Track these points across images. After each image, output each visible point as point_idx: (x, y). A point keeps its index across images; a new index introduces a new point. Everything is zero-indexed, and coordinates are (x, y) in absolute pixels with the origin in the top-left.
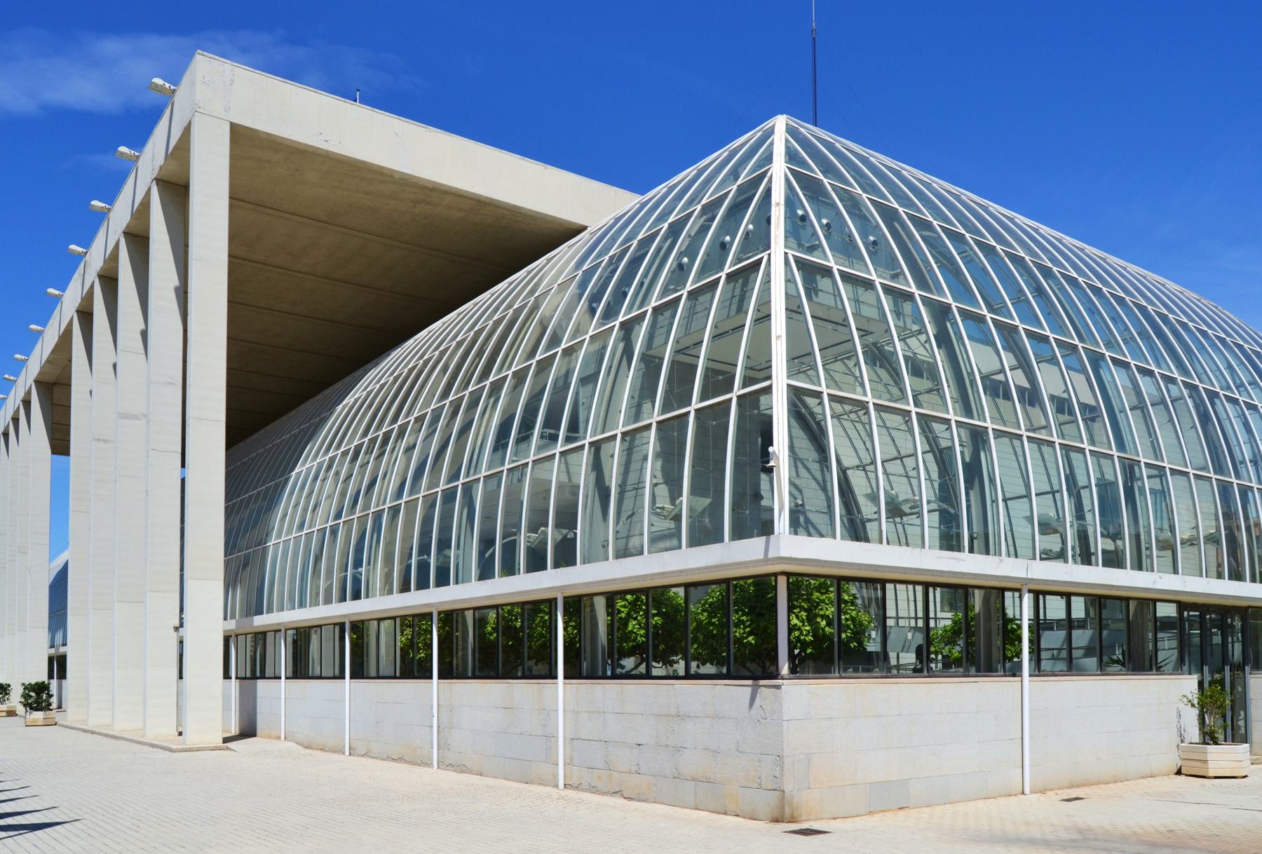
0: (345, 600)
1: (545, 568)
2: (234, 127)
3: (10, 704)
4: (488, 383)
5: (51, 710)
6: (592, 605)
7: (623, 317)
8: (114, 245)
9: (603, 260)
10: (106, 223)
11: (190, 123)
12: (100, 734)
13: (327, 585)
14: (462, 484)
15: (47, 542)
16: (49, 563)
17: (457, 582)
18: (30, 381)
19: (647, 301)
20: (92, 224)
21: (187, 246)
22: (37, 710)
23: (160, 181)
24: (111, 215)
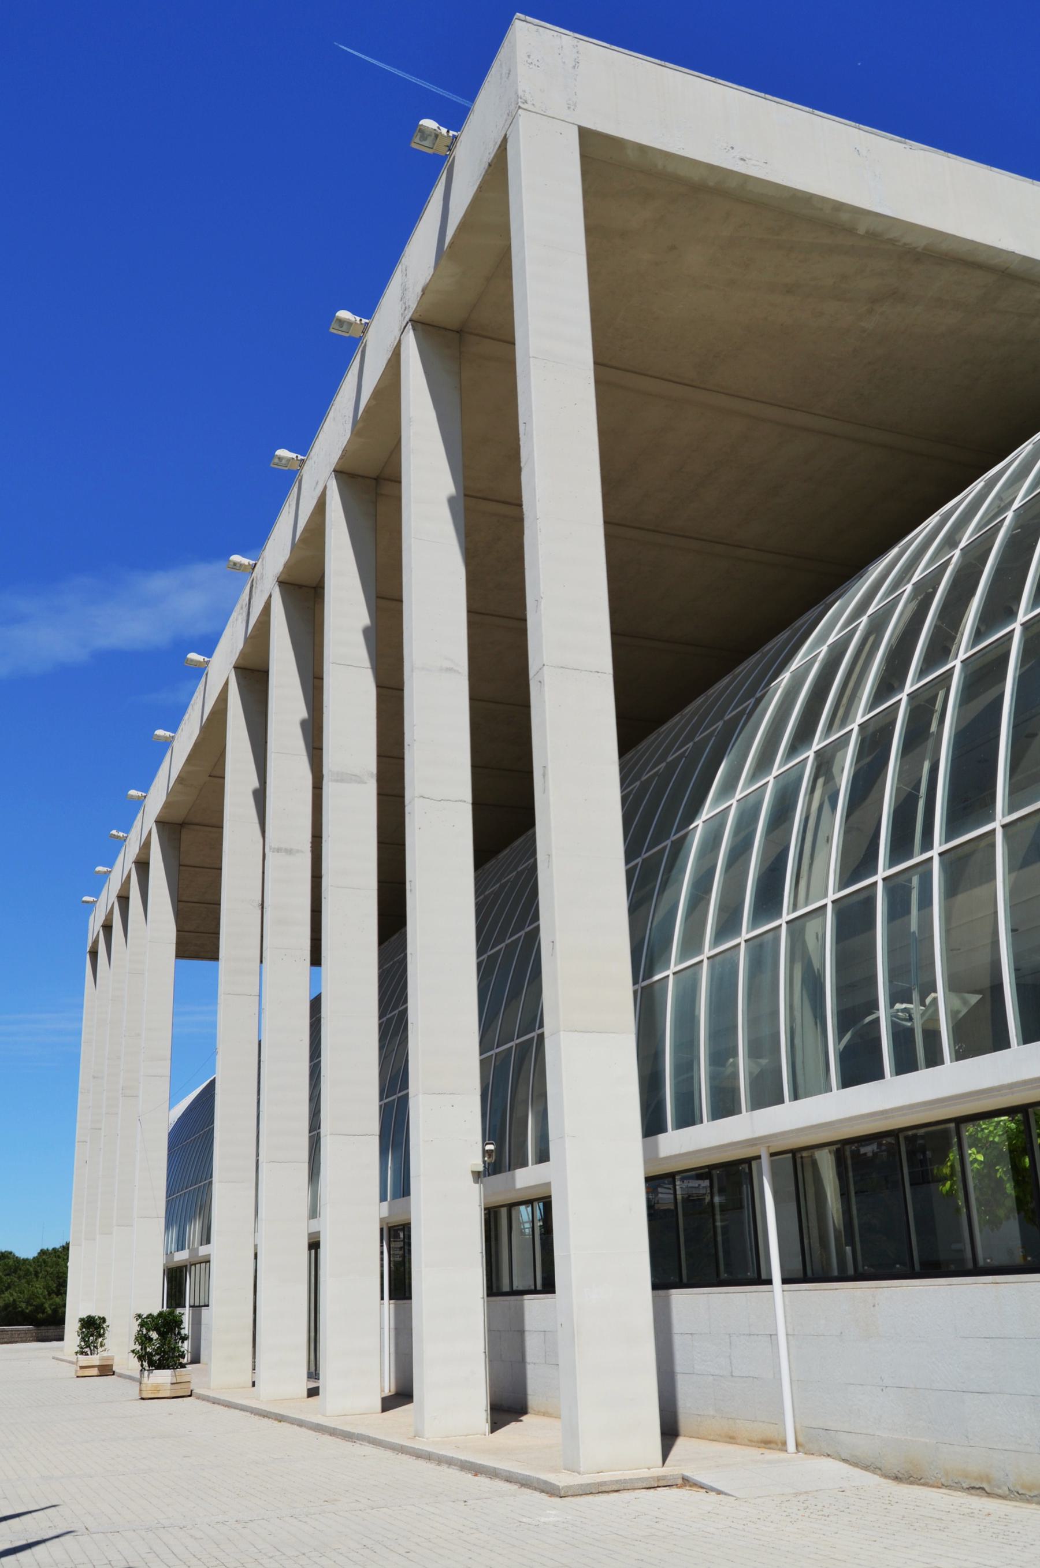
0: (940, 1061)
1: (1006, 1045)
2: (586, 135)
3: (105, 1354)
4: (810, 754)
5: (183, 1366)
6: (814, 1163)
7: (818, 744)
8: (224, 682)
9: (905, 591)
10: (295, 490)
11: (505, 140)
12: (301, 1424)
13: (923, 1021)
14: (833, 902)
15: (167, 1072)
16: (169, 1110)
17: (796, 1097)
18: (230, 666)
19: (851, 716)
20: (98, 883)
21: (266, 742)
22: (160, 1366)
23: (344, 474)
24: (175, 744)
